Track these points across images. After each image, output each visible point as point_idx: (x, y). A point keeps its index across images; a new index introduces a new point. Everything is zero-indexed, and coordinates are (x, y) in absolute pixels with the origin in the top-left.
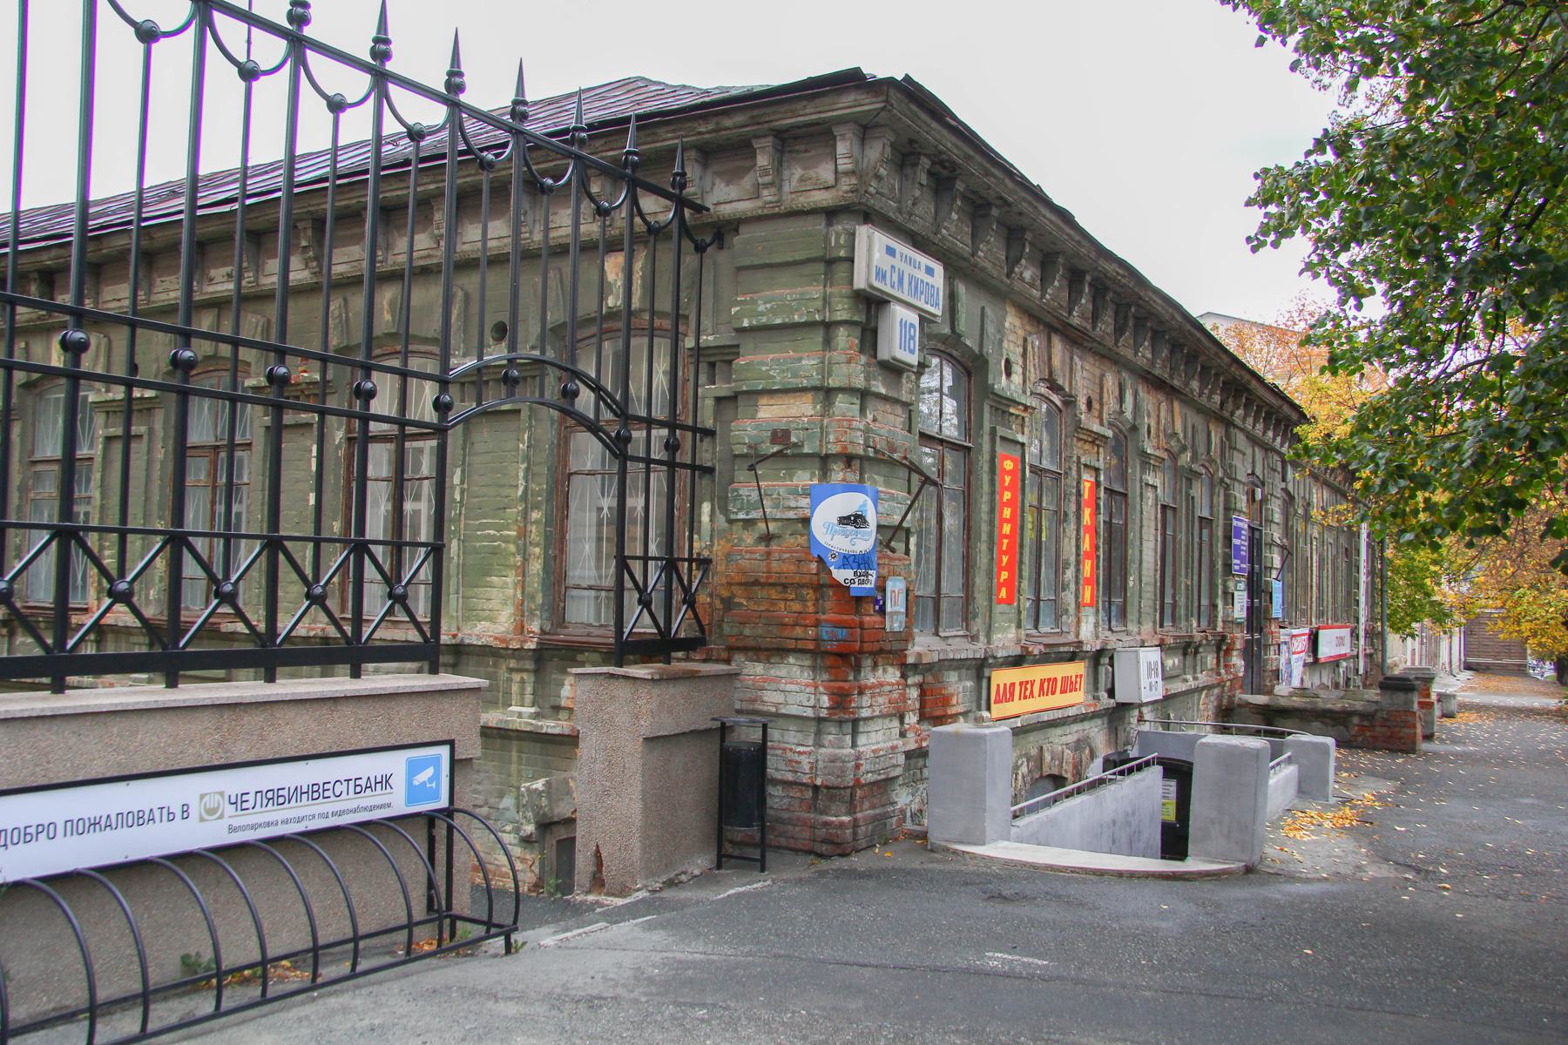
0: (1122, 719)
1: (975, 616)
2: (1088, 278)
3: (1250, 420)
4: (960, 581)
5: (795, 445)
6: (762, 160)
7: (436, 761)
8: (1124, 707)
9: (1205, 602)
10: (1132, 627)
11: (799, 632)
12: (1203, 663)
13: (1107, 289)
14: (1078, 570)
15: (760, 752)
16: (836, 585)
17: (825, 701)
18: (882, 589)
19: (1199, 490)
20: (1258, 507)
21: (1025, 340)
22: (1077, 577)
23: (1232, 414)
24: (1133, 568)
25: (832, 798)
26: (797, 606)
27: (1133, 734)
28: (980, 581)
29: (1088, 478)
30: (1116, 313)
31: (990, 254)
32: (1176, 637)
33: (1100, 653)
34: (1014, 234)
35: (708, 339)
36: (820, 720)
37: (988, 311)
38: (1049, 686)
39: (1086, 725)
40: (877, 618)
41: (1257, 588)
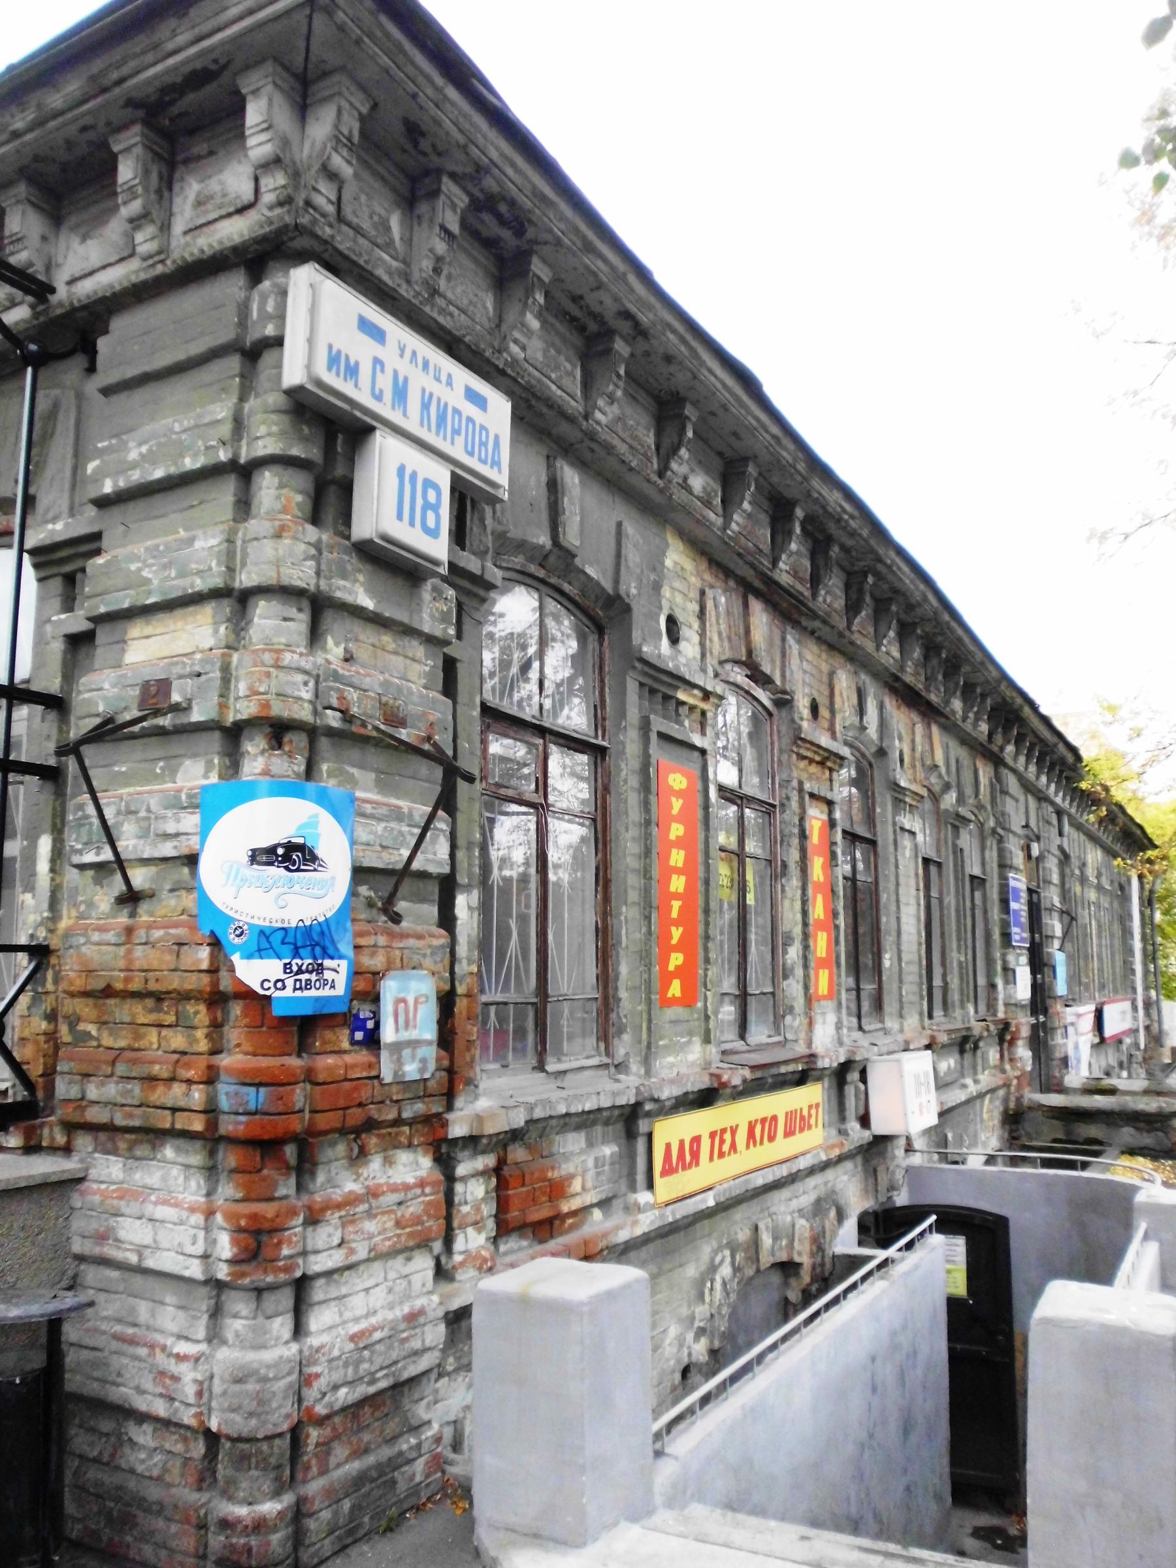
0: (882, 1154)
1: (621, 1031)
2: (799, 513)
3: (1022, 759)
4: (591, 971)
5: (176, 708)
8: (881, 1142)
9: (982, 981)
10: (891, 1023)
11: (176, 1093)
12: (985, 1059)
13: (829, 539)
14: (806, 947)
16: (246, 994)
17: (225, 1247)
19: (967, 840)
20: (1035, 863)
21: (703, 593)
22: (805, 958)
23: (1002, 749)
24: (888, 941)
25: (242, 1461)
26: (177, 1040)
27: (899, 1175)
28: (625, 969)
29: (816, 817)
30: (847, 587)
31: (617, 416)
32: (950, 1032)
33: (841, 1073)
34: (666, 408)
36: (219, 1286)
37: (629, 529)
39: (830, 1174)
40: (363, 1056)
41: (1039, 963)
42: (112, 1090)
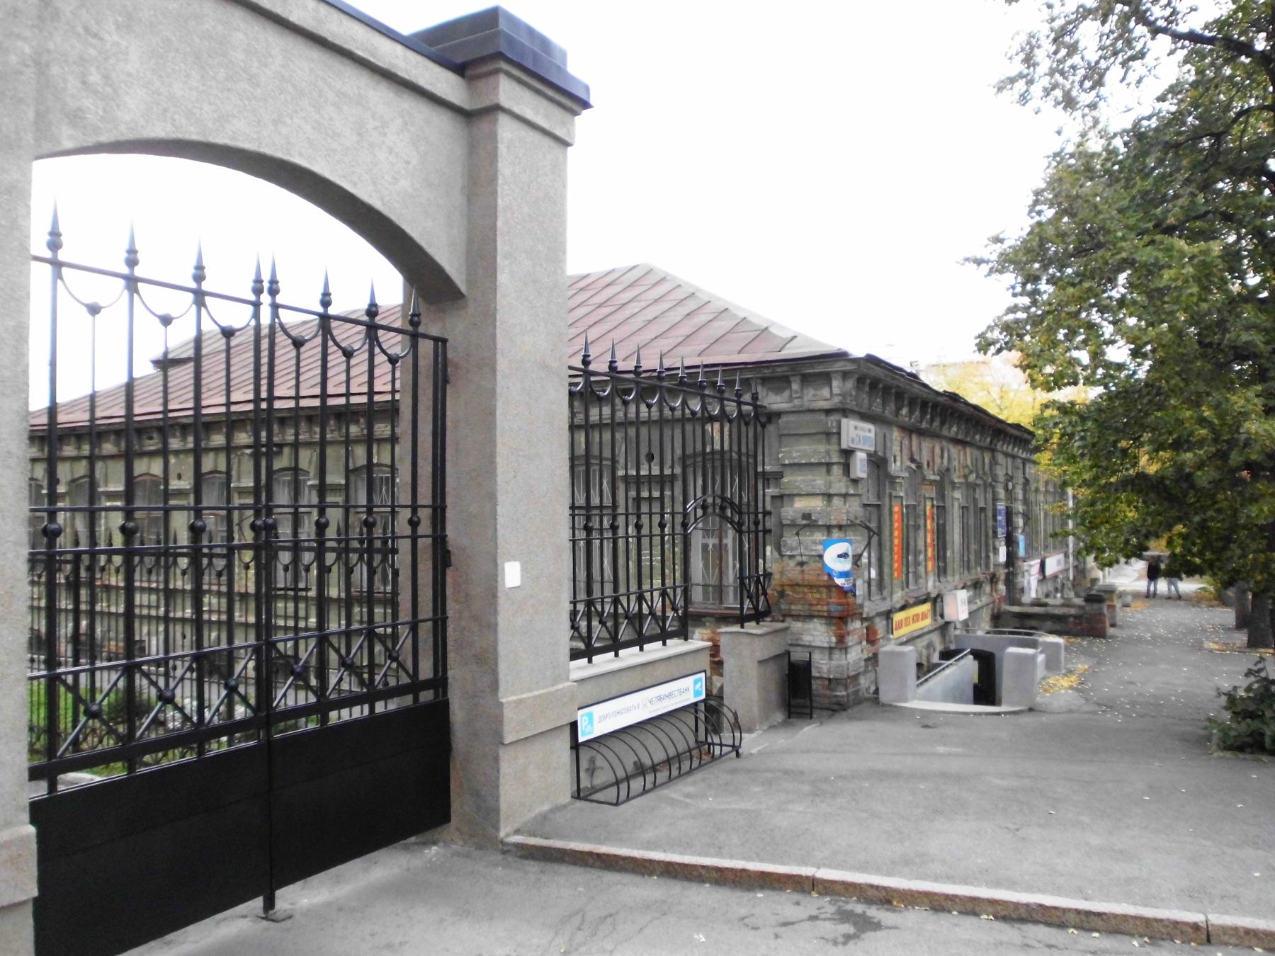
6: (795, 386)
7: (700, 679)
8: (948, 623)
10: (949, 578)
11: (819, 607)
15: (808, 665)
16: (837, 586)
17: (834, 639)
18: (854, 585)
19: (979, 494)
20: (1010, 494)
24: (949, 546)
26: (817, 596)
35: (768, 468)
38: (916, 618)
41: (1010, 541)
42: (799, 607)
